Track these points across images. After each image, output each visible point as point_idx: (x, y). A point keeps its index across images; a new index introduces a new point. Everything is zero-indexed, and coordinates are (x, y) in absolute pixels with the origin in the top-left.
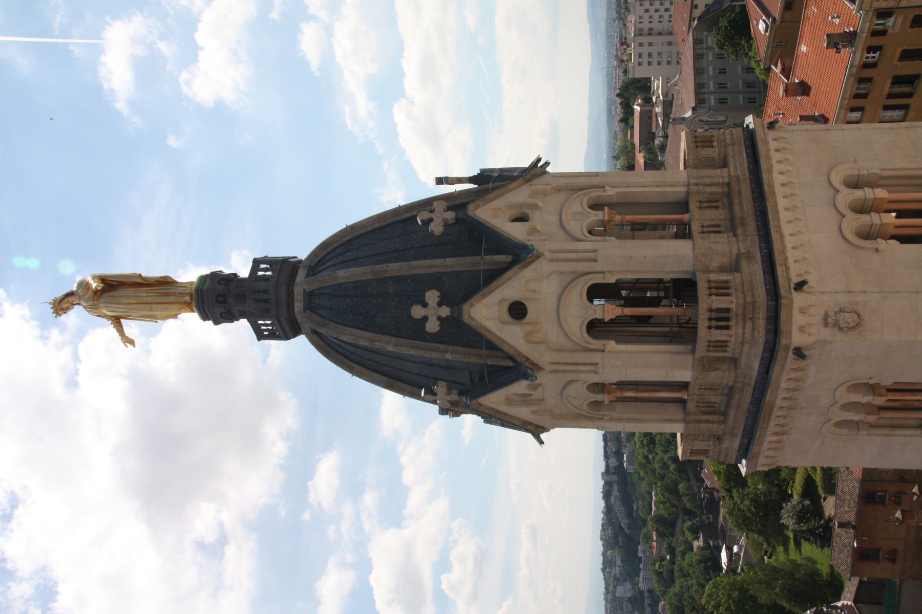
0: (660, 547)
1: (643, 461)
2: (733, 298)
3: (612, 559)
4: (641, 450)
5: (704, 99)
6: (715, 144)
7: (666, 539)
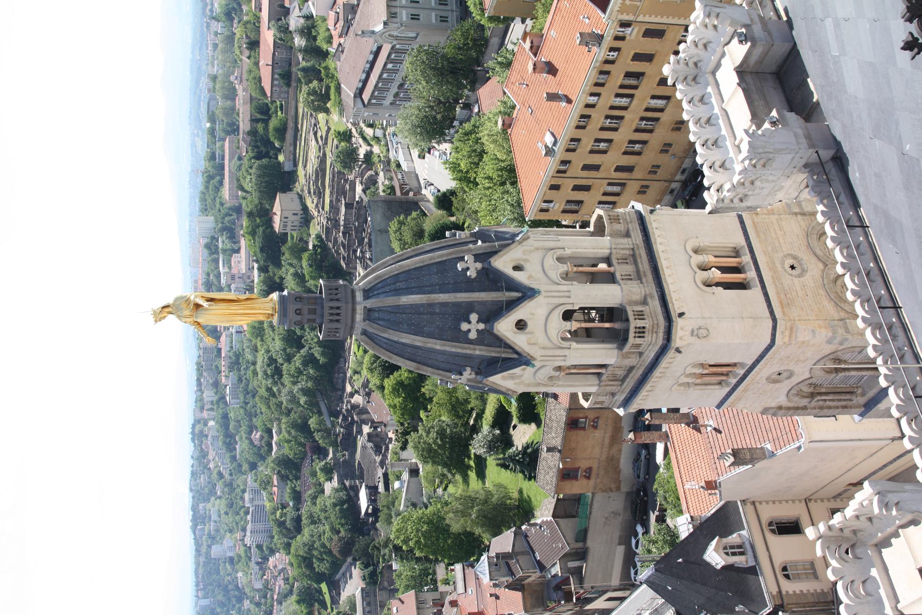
0: (282, 492)
1: (266, 394)
2: (646, 321)
3: (205, 513)
4: (264, 382)
5: (395, 14)
6: (621, 221)
7: (289, 483)
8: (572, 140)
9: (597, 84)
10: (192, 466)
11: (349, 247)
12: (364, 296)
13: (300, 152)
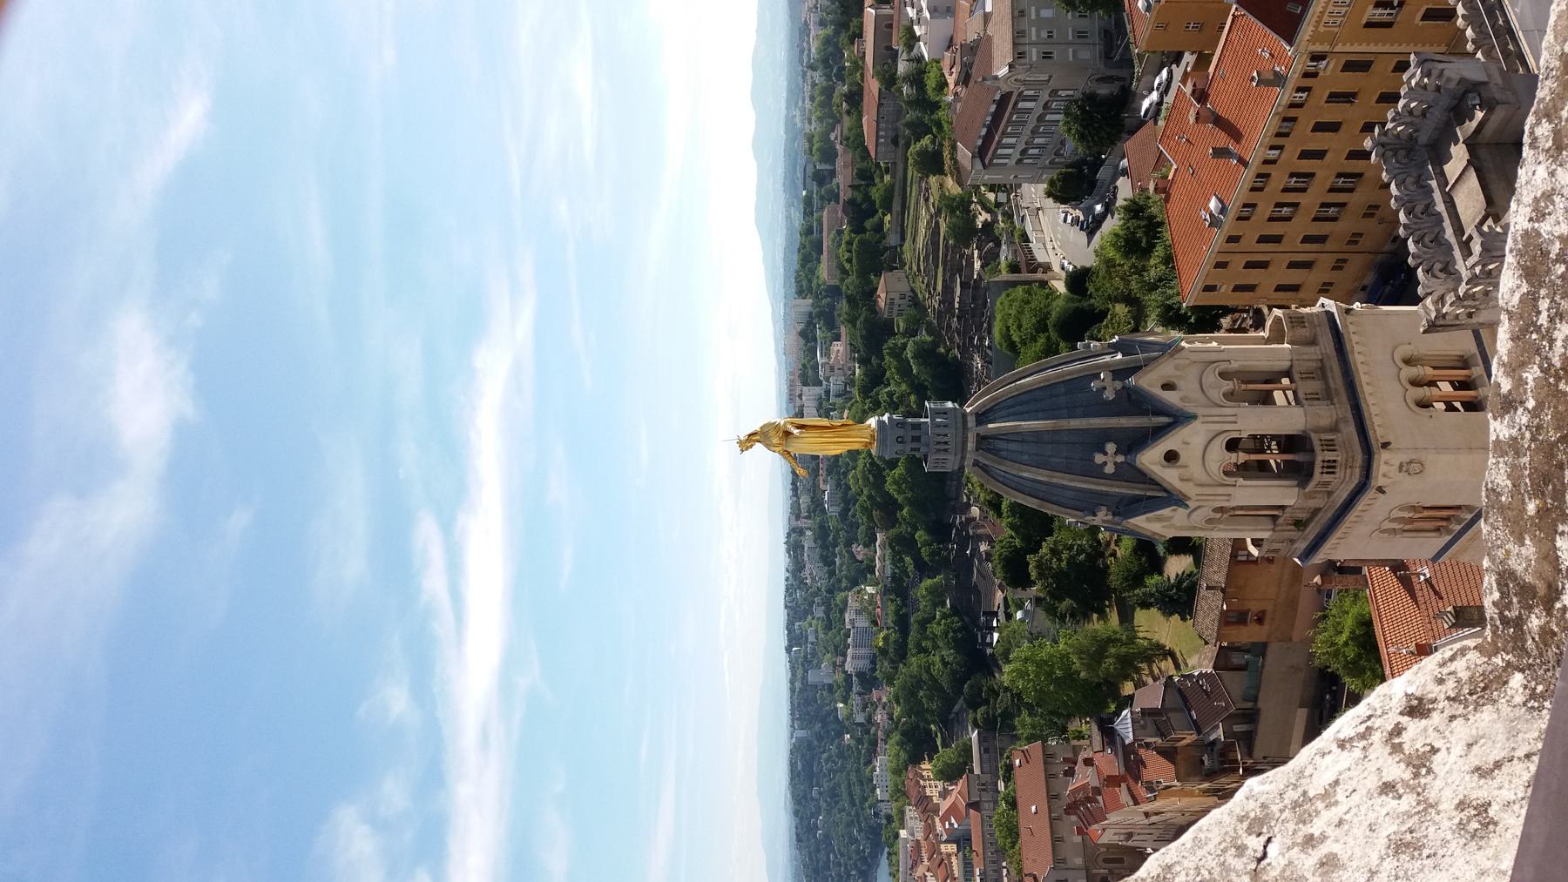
3: (801, 633)
5: (1024, 53)
6: (1306, 324)
8: (1245, 206)
9: (1278, 135)
10: (787, 579)
11: (965, 333)
12: (977, 421)
13: (909, 223)
